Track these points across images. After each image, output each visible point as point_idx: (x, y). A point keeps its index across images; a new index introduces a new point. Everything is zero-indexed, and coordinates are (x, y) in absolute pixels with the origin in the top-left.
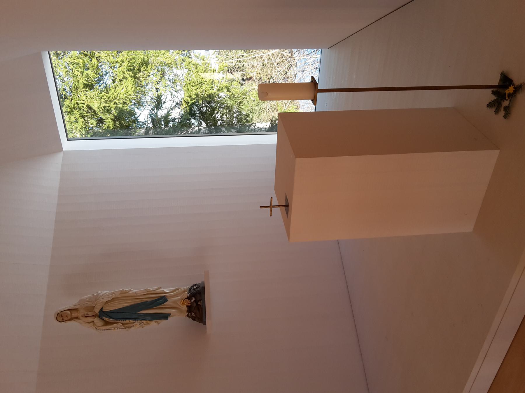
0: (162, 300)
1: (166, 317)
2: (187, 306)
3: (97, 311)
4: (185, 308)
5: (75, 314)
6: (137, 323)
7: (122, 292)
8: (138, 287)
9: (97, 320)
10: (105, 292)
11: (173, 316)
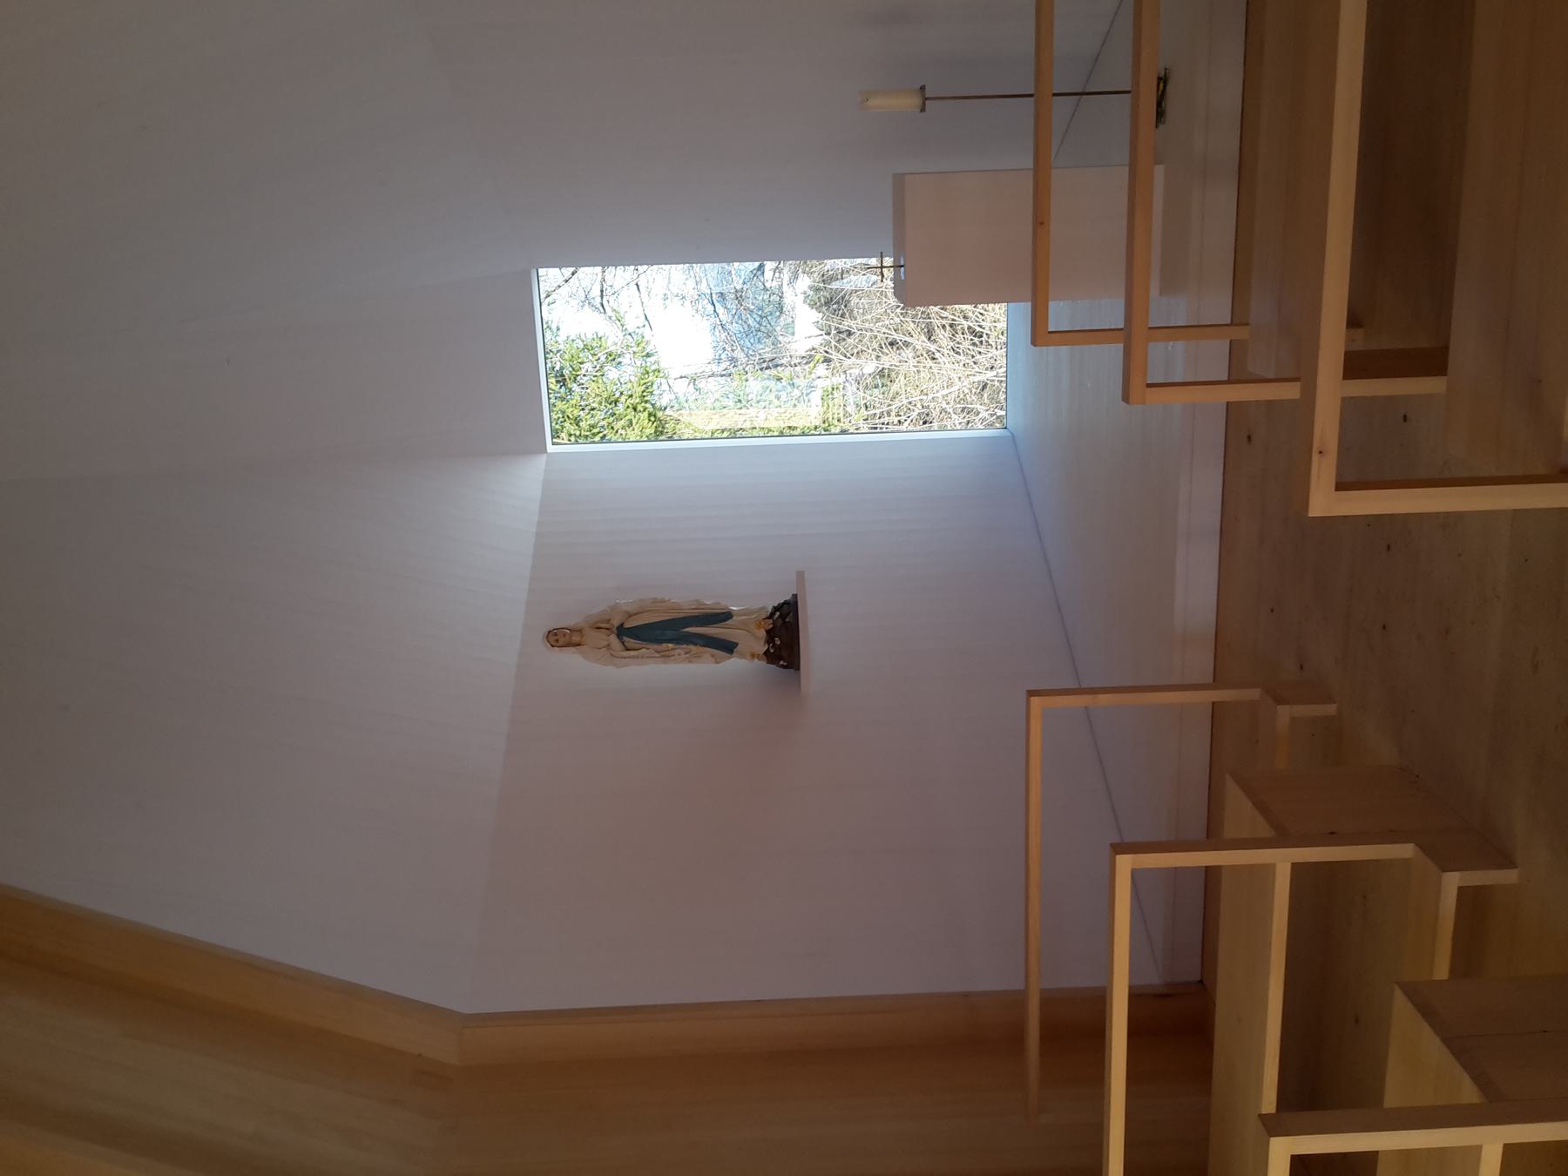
0: (724, 617)
1: (728, 647)
2: (768, 632)
3: (616, 623)
4: (762, 633)
5: (576, 638)
6: (680, 650)
7: (655, 601)
8: (684, 596)
9: (613, 639)
10: (627, 601)
11: (742, 656)
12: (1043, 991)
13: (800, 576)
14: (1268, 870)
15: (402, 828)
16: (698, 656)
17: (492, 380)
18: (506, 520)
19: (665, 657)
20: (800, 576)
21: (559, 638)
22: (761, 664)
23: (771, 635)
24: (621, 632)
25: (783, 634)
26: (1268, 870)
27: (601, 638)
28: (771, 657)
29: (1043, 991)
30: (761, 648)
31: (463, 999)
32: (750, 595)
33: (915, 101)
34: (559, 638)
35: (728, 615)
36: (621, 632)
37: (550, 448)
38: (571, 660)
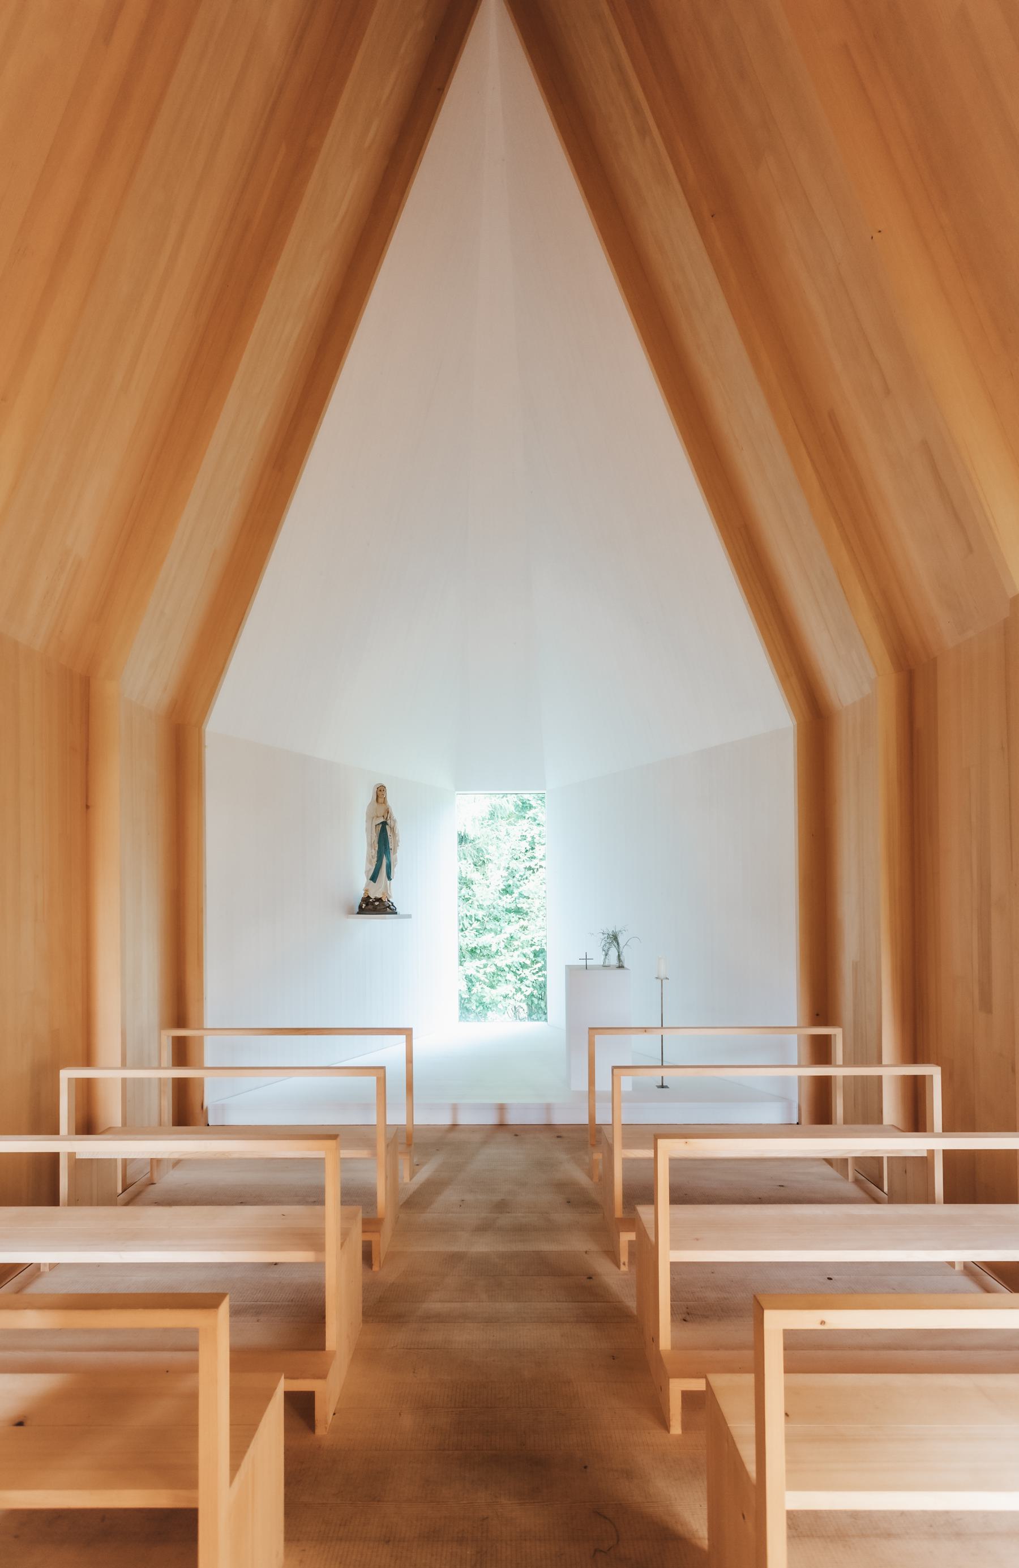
1: (374, 878)
4: (379, 896)
5: (380, 800)
6: (374, 853)
9: (382, 820)
10: (393, 829)
11: (367, 885)
12: (672, 1160)
13: (409, 916)
15: (498, 411)
16: (370, 862)
20: (409, 916)
21: (380, 792)
22: (361, 894)
23: (380, 900)
24: (384, 824)
25: (373, 906)
27: (381, 811)
28: (366, 900)
29: (672, 1160)
32: (396, 891)
33: (662, 976)
34: (380, 792)
35: (389, 878)
36: (384, 824)
38: (365, 798)
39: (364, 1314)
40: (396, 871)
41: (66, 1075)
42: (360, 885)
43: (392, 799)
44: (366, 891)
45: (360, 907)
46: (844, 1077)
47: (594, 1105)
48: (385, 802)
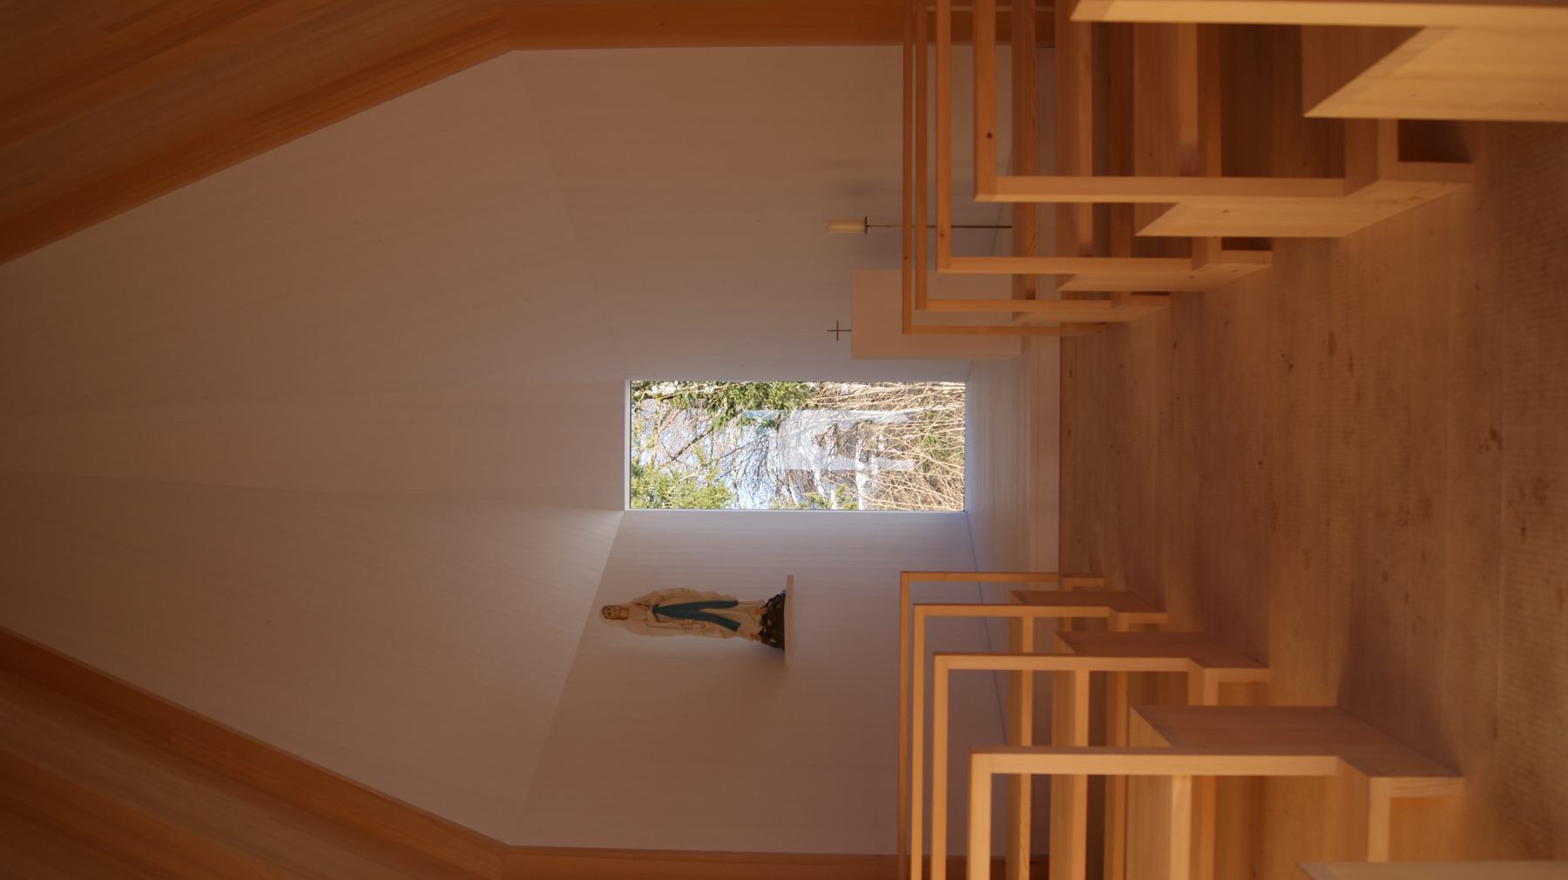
1: (733, 626)
3: (653, 603)
4: (759, 617)
6: (697, 625)
9: (650, 613)
10: (663, 599)
11: (744, 635)
13: (790, 579)
14: (1067, 677)
17: (599, 468)
18: (589, 549)
19: (686, 629)
20: (790, 579)
21: (612, 613)
22: (758, 643)
23: (764, 618)
24: (657, 610)
25: (773, 622)
26: (1067, 677)
30: (757, 629)
31: (510, 836)
35: (735, 603)
36: (657, 610)
37: (627, 507)
38: (621, 635)
39: (1326, 174)
40: (724, 593)
41: (985, 767)
42: (742, 644)
43: (623, 598)
44: (752, 636)
45: (775, 646)
46: (1035, 672)
47: (1047, 846)
48: (621, 608)
